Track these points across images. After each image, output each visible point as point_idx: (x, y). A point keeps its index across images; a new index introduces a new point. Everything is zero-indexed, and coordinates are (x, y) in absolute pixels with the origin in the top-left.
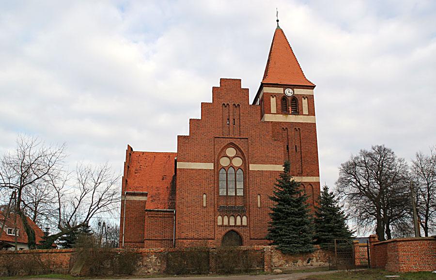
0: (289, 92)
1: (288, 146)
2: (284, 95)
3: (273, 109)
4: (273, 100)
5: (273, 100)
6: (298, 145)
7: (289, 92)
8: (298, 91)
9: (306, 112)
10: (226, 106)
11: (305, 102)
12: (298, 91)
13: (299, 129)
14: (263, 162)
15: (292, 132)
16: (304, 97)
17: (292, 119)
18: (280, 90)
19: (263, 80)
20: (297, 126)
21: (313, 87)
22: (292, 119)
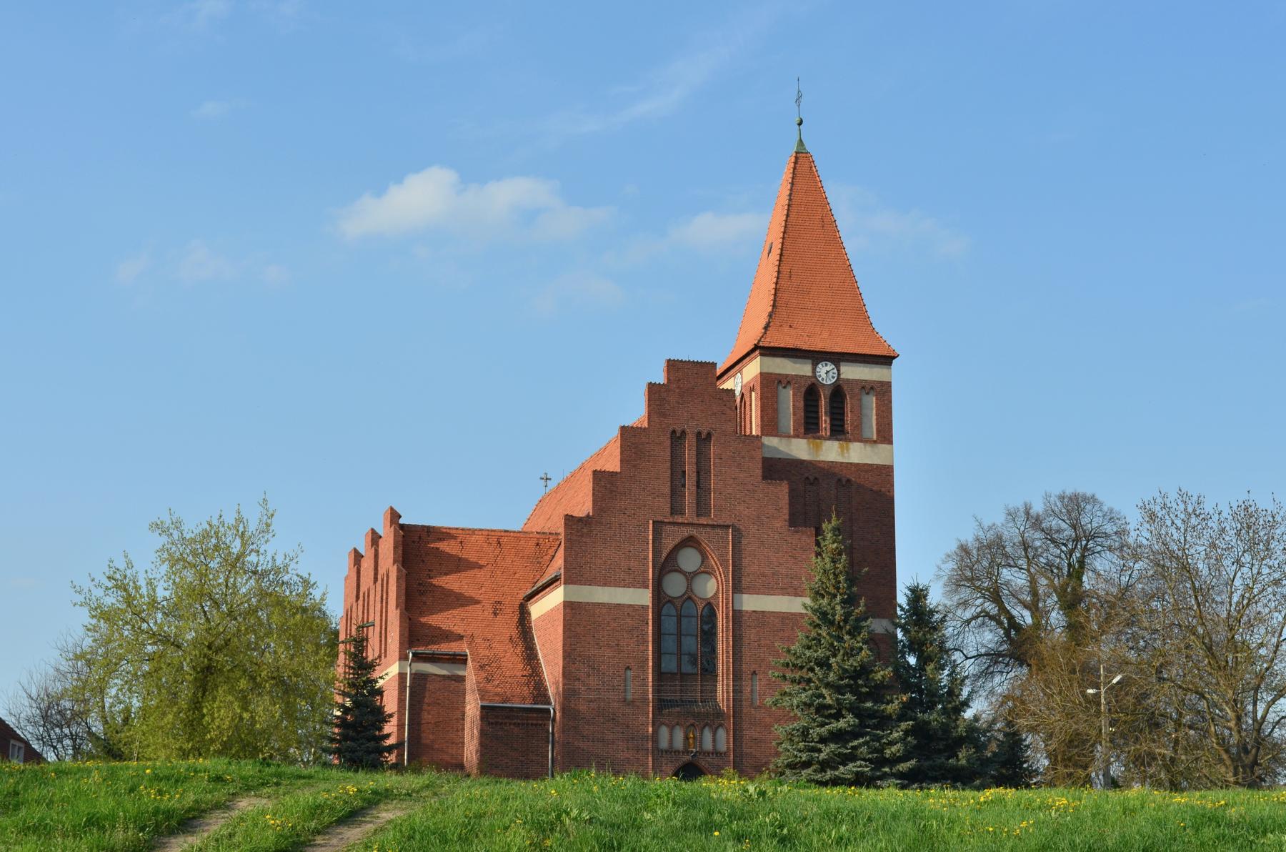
0: (826, 373)
2: (813, 380)
7: (826, 373)
8: (852, 372)
11: (871, 402)
12: (852, 372)
14: (768, 590)
16: (868, 387)
17: (831, 452)
19: (766, 328)
20: (838, 478)
21: (886, 360)
22: (831, 452)
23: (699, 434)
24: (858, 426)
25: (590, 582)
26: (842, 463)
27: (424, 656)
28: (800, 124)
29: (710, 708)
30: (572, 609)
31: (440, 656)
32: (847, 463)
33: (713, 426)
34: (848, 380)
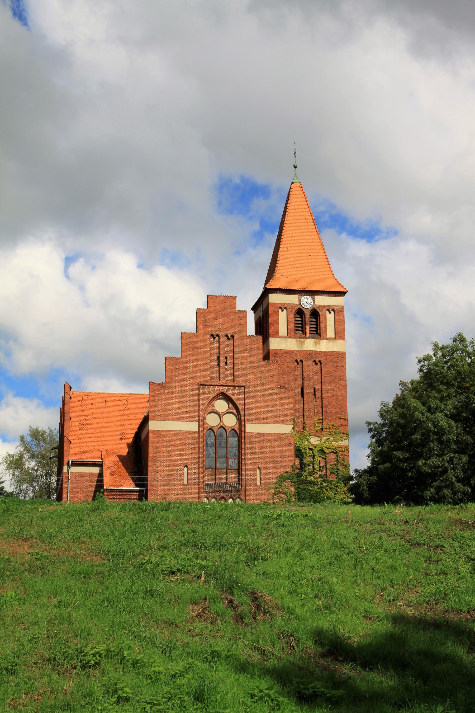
1: (302, 389)
2: (300, 306)
3: (283, 330)
4: (282, 315)
5: (282, 315)
6: (318, 387)
8: (321, 301)
9: (330, 333)
10: (214, 338)
11: (330, 318)
13: (320, 361)
14: (265, 421)
15: (310, 368)
16: (330, 309)
18: (292, 299)
23: (227, 336)
24: (278, 332)
25: (165, 419)
26: (316, 351)
27: (78, 462)
28: (295, 167)
29: (233, 487)
30: (154, 434)
31: (87, 463)
32: (319, 351)
33: (234, 331)
34: (319, 305)
